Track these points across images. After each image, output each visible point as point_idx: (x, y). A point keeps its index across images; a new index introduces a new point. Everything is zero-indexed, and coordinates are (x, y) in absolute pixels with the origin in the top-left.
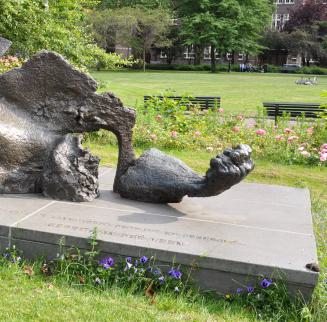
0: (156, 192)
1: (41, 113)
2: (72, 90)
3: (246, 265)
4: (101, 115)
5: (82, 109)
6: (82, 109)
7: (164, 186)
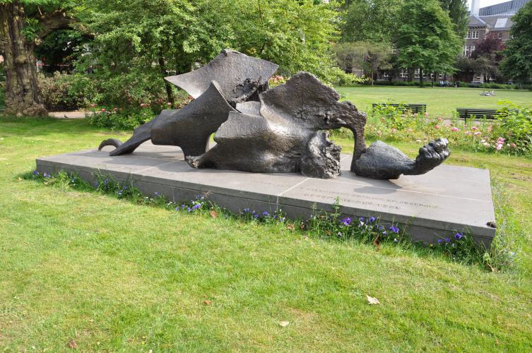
0: (381, 171)
1: (299, 116)
2: (322, 100)
3: (444, 223)
4: (342, 117)
5: (329, 113)
6: (329, 113)
7: (386, 167)
